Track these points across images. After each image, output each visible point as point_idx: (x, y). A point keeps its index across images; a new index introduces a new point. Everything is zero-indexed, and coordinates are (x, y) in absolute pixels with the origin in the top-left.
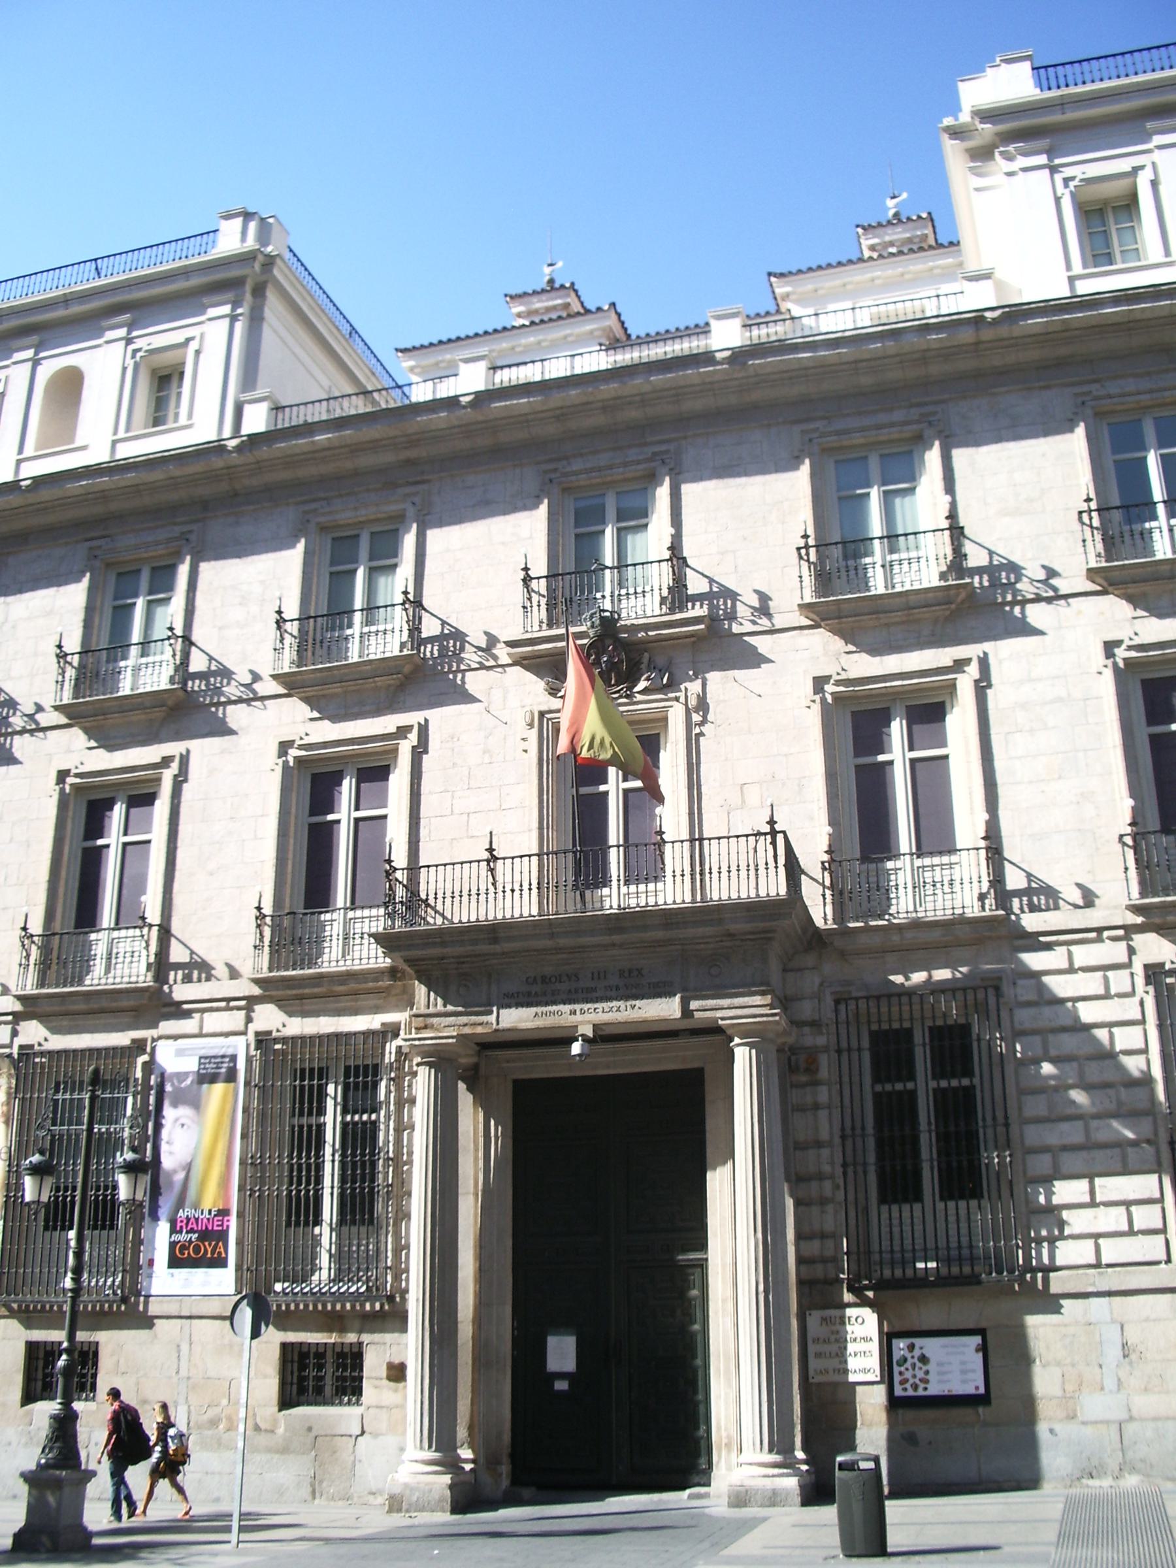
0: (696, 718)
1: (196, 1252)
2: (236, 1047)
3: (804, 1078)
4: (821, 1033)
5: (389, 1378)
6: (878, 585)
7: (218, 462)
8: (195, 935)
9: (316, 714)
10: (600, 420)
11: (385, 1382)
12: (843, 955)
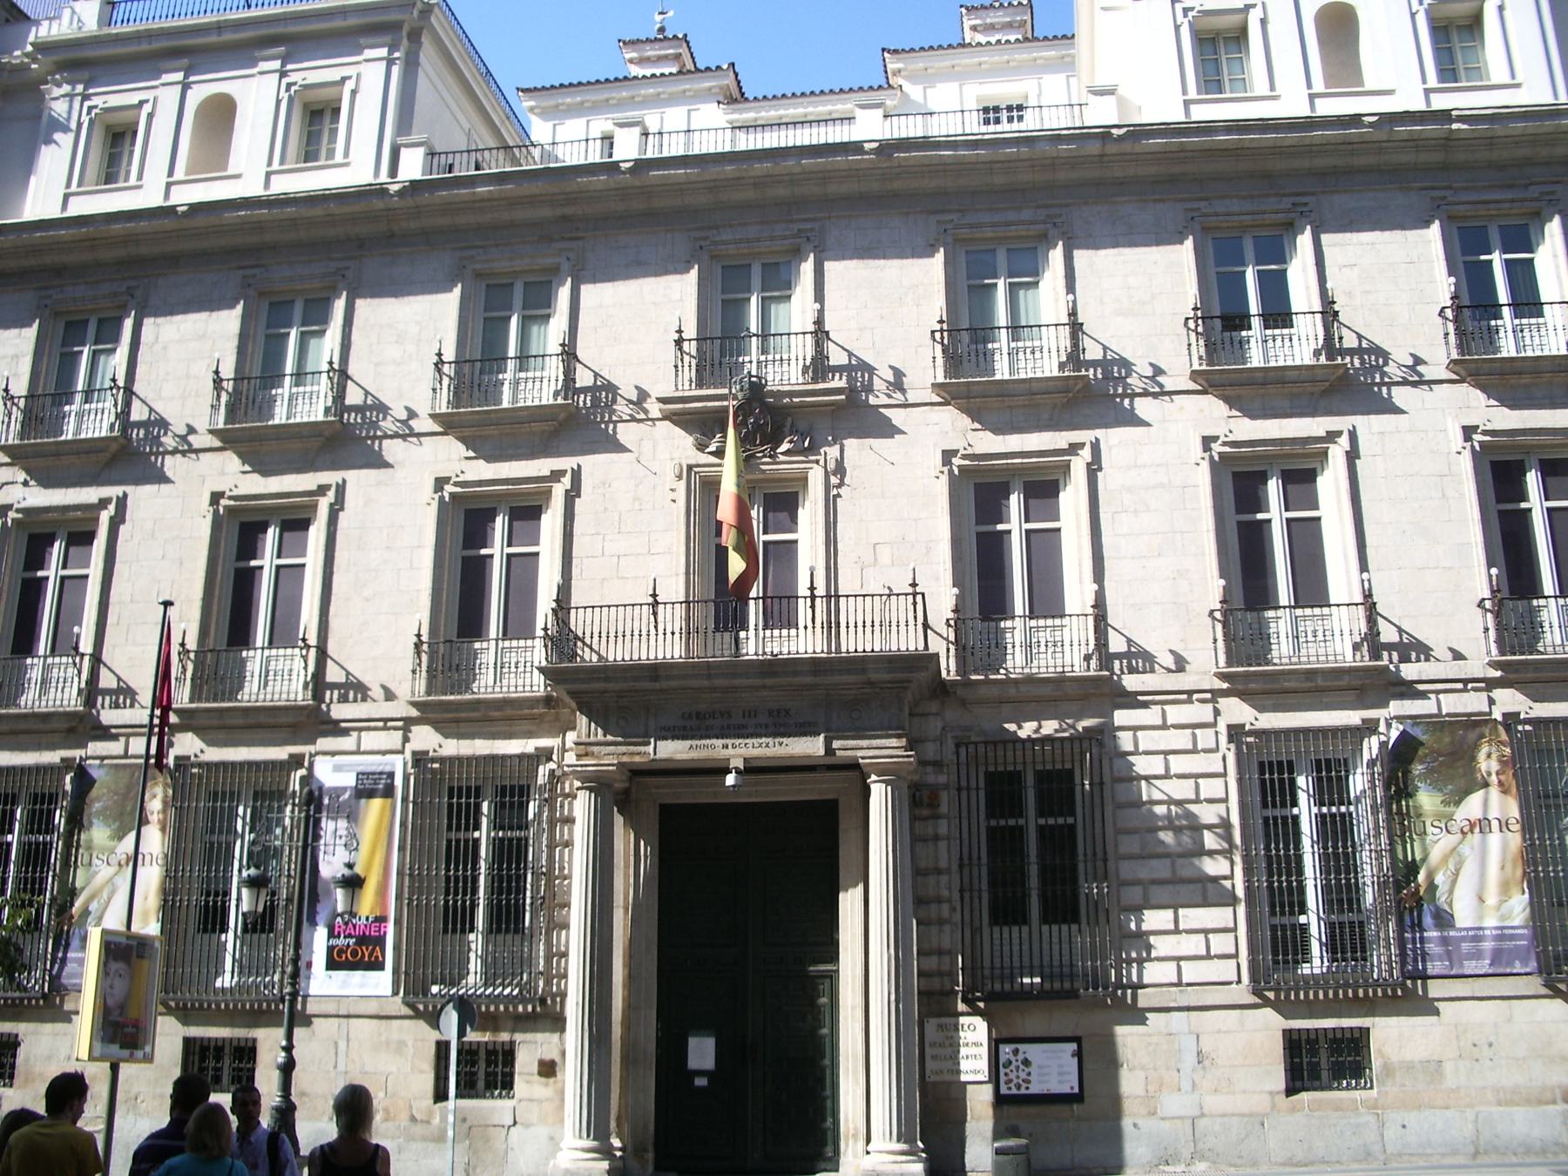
0: (834, 480)
1: (356, 954)
2: (393, 765)
3: (925, 812)
4: (942, 772)
5: (540, 1074)
6: (1002, 371)
7: (378, 204)
9: (471, 454)
10: (750, 194)
11: (537, 1077)
12: (963, 703)
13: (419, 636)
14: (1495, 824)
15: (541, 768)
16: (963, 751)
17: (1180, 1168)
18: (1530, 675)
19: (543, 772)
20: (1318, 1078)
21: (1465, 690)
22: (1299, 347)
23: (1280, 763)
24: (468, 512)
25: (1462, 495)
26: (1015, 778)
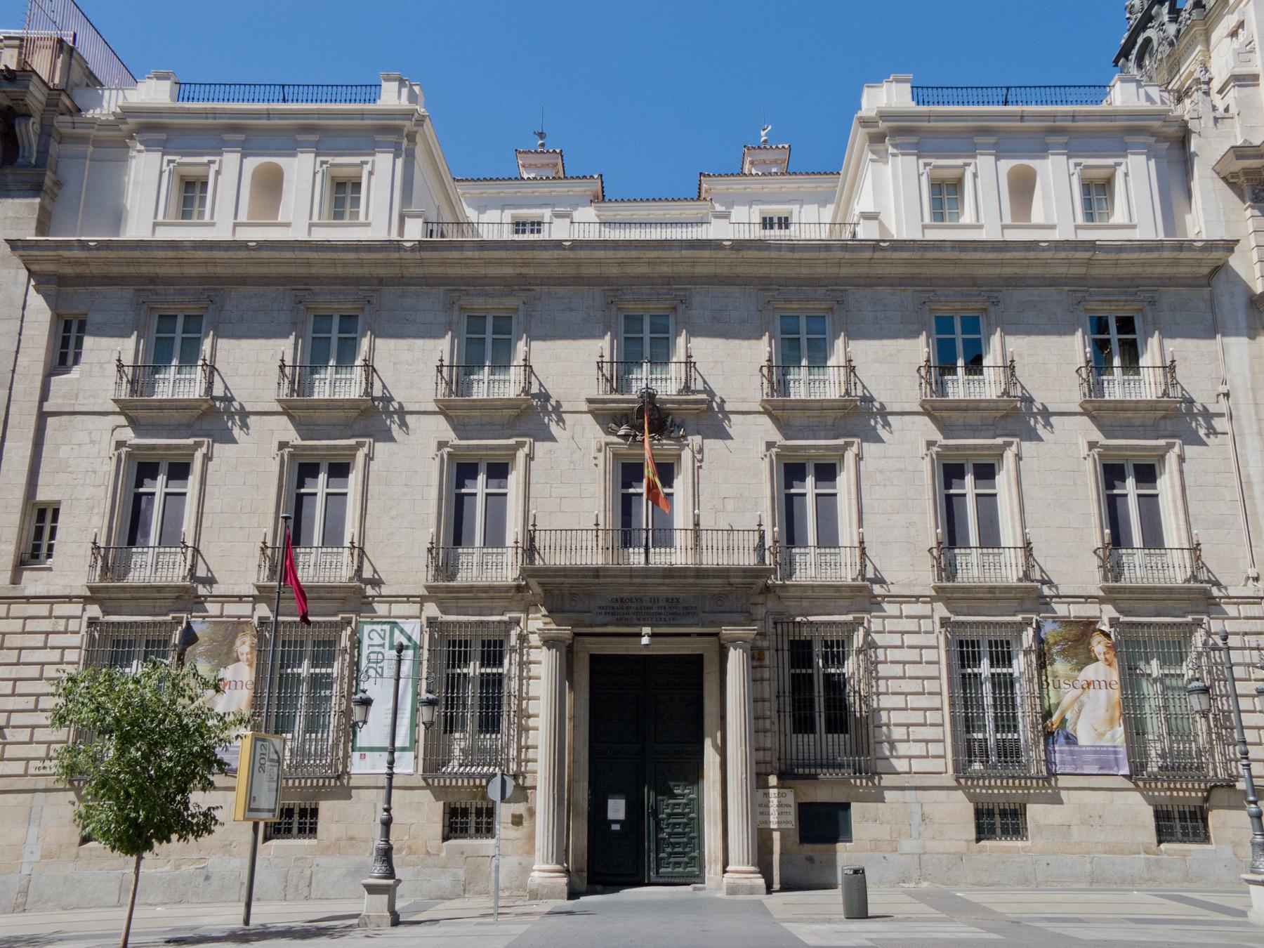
0: (699, 457)
5: (513, 823)
8: (215, 556)
13: (264, 543)
14: (1103, 684)
15: (513, 633)
16: (779, 627)
17: (912, 885)
18: (1127, 596)
19: (514, 633)
20: (994, 832)
21: (1086, 602)
22: (989, 386)
23: (460, 642)
24: (301, 465)
25: (1086, 484)
26: (808, 644)
